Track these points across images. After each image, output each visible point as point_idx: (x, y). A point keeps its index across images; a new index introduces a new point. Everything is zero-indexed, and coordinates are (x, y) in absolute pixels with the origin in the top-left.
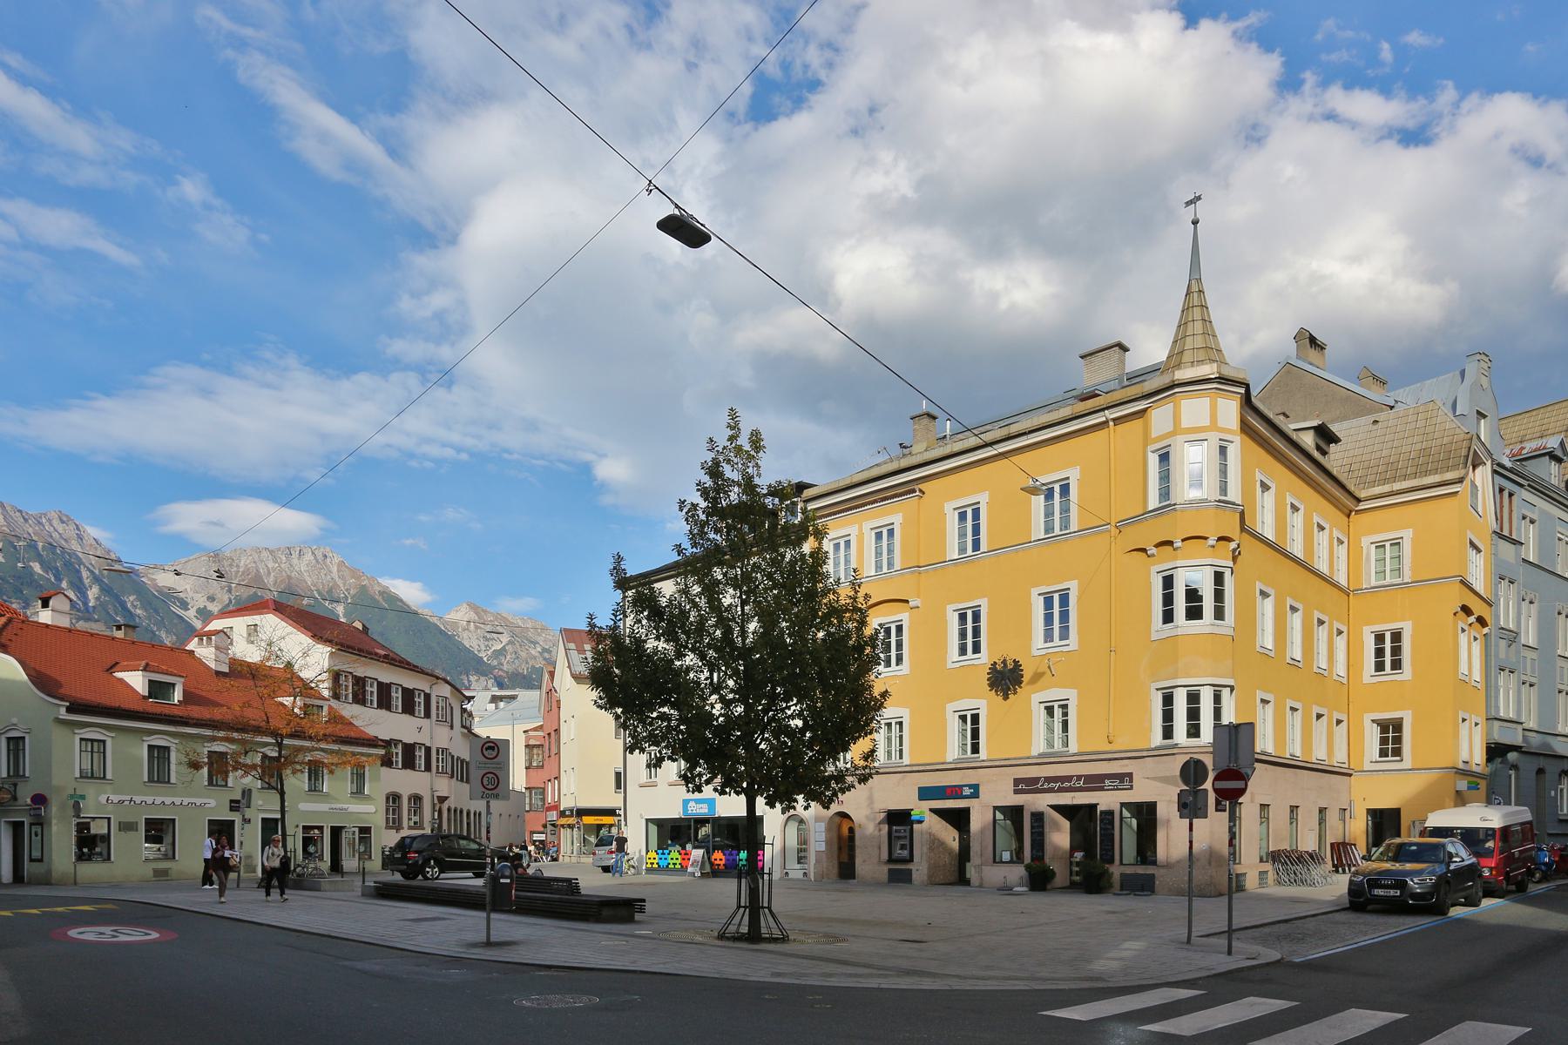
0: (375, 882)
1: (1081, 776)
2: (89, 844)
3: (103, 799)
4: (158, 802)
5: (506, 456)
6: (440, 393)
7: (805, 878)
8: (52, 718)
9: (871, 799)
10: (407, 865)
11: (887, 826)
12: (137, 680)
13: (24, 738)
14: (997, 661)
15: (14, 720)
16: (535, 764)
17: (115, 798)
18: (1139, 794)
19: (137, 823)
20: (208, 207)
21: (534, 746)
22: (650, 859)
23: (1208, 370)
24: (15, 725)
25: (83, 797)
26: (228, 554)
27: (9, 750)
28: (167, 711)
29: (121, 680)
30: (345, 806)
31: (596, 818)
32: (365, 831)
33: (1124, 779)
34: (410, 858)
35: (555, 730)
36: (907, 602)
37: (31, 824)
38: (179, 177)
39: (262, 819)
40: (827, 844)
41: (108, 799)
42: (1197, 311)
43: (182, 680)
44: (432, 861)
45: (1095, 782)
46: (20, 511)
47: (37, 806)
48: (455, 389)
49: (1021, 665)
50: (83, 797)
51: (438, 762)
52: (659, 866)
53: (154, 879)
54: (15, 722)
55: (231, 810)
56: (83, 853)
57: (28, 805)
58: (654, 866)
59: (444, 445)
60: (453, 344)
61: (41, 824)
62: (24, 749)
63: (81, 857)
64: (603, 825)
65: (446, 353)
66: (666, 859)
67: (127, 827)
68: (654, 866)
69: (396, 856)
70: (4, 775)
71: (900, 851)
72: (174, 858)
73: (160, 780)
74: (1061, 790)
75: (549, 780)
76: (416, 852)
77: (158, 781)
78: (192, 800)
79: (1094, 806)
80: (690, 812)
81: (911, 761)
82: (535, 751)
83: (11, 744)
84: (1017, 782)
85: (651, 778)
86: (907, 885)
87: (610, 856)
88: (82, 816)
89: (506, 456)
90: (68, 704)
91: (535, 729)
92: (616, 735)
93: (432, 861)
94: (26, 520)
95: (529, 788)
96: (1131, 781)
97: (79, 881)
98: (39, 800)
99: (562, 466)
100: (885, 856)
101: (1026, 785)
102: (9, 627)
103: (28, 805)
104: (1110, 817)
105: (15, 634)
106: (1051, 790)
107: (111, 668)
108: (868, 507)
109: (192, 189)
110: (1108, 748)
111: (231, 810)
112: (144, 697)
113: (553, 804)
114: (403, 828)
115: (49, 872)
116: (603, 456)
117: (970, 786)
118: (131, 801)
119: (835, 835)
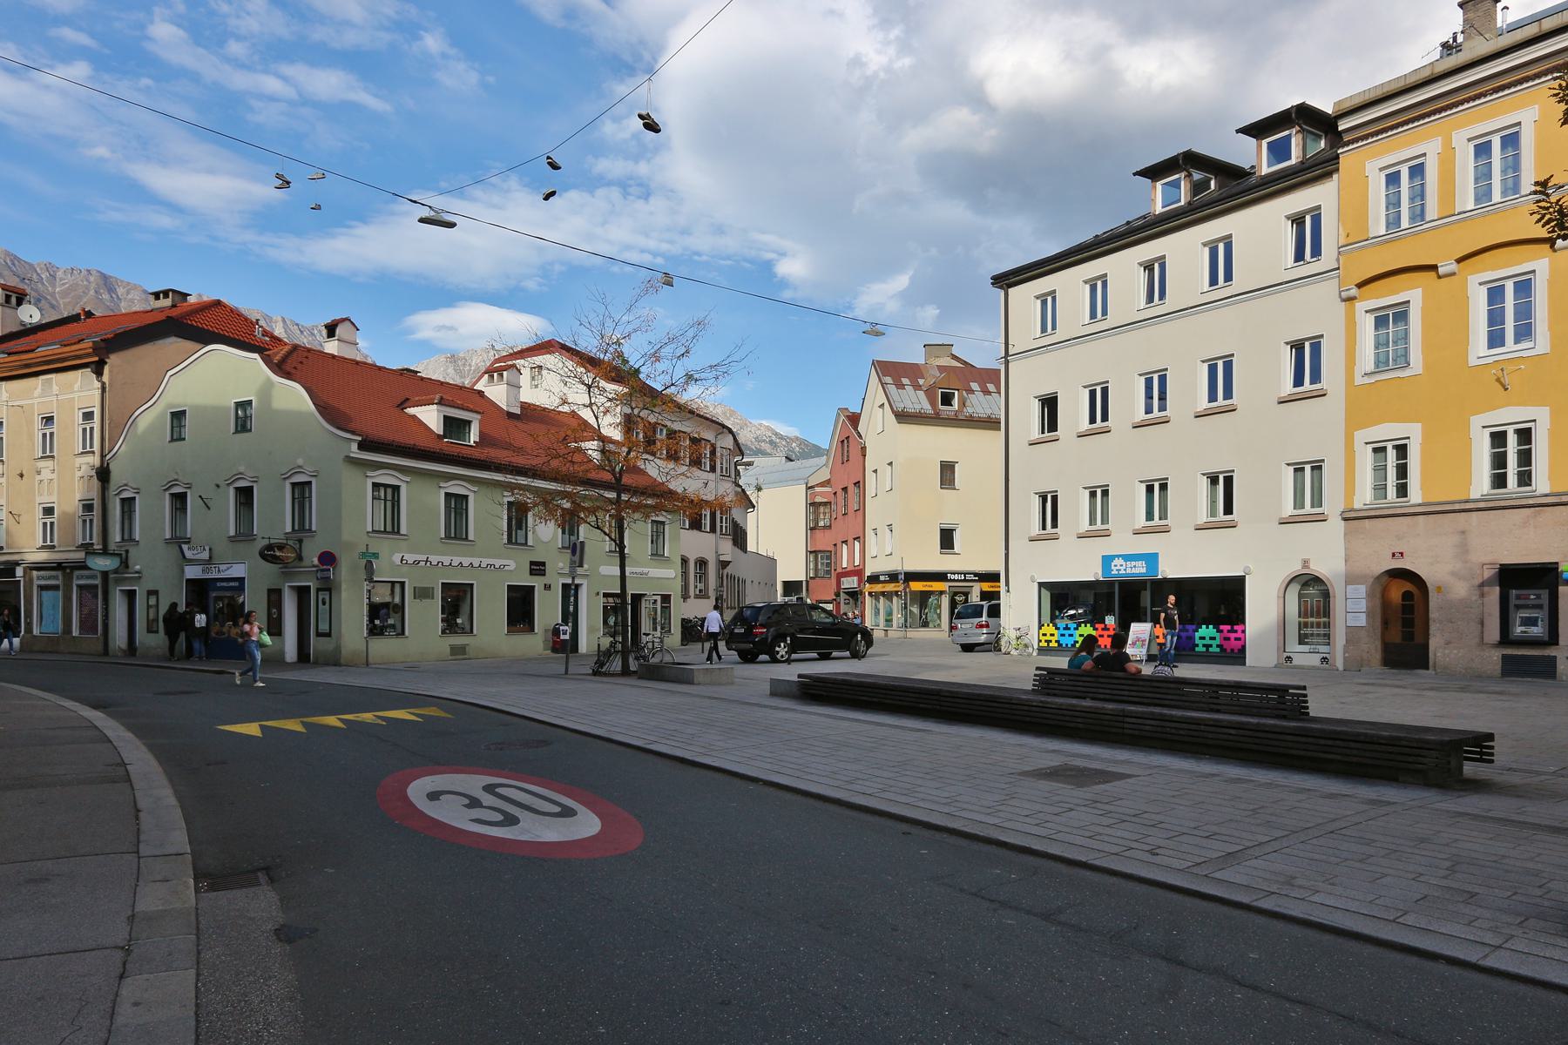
0: (800, 676)
2: (383, 618)
3: (397, 558)
4: (454, 563)
5: (696, 258)
6: (640, 204)
7: (1325, 665)
8: (342, 456)
9: (1463, 549)
10: (754, 643)
11: (1497, 589)
12: (431, 416)
13: (310, 483)
15: (300, 462)
16: (821, 524)
17: (410, 558)
19: (433, 588)
20: (444, 56)
21: (821, 504)
22: (1044, 635)
24: (300, 467)
25: (376, 556)
26: (461, 355)
27: (293, 499)
28: (465, 452)
29: (414, 417)
30: (646, 570)
31: (925, 583)
32: (666, 599)
34: (756, 635)
35: (857, 484)
36: (1434, 268)
37: (318, 590)
38: (422, 32)
39: (563, 584)
40: (1368, 616)
41: (402, 560)
43: (479, 417)
44: (859, 636)
46: (297, 325)
47: (325, 567)
48: (652, 200)
50: (376, 556)
51: (721, 522)
52: (1060, 645)
53: (450, 658)
54: (300, 464)
55: (531, 574)
56: (376, 625)
57: (314, 566)
58: (1051, 645)
59: (642, 251)
60: (649, 161)
61: (329, 590)
62: (310, 497)
63: (374, 631)
64: (931, 593)
65: (643, 169)
66: (1071, 635)
67: (423, 593)
68: (1051, 645)
69: (736, 631)
70: (289, 529)
71: (1523, 629)
72: (472, 631)
73: (458, 536)
75: (845, 542)
76: (762, 626)
77: (455, 538)
78: (491, 561)
80: (1114, 572)
81: (1423, 498)
82: (822, 509)
83: (296, 491)
86: (1550, 681)
87: (979, 631)
88: (375, 579)
89: (696, 258)
90: (360, 439)
91: (822, 485)
92: (941, 484)
93: (859, 636)
94: (302, 332)
95: (814, 552)
97: (370, 660)
98: (328, 559)
99: (747, 265)
100: (1493, 633)
102: (295, 354)
103: (314, 566)
105: (301, 363)
107: (402, 404)
108: (1466, 106)
109: (433, 42)
111: (531, 574)
112: (439, 436)
113: (851, 568)
114: (690, 597)
115: (338, 649)
116: (783, 254)
118: (427, 561)
119: (1378, 602)
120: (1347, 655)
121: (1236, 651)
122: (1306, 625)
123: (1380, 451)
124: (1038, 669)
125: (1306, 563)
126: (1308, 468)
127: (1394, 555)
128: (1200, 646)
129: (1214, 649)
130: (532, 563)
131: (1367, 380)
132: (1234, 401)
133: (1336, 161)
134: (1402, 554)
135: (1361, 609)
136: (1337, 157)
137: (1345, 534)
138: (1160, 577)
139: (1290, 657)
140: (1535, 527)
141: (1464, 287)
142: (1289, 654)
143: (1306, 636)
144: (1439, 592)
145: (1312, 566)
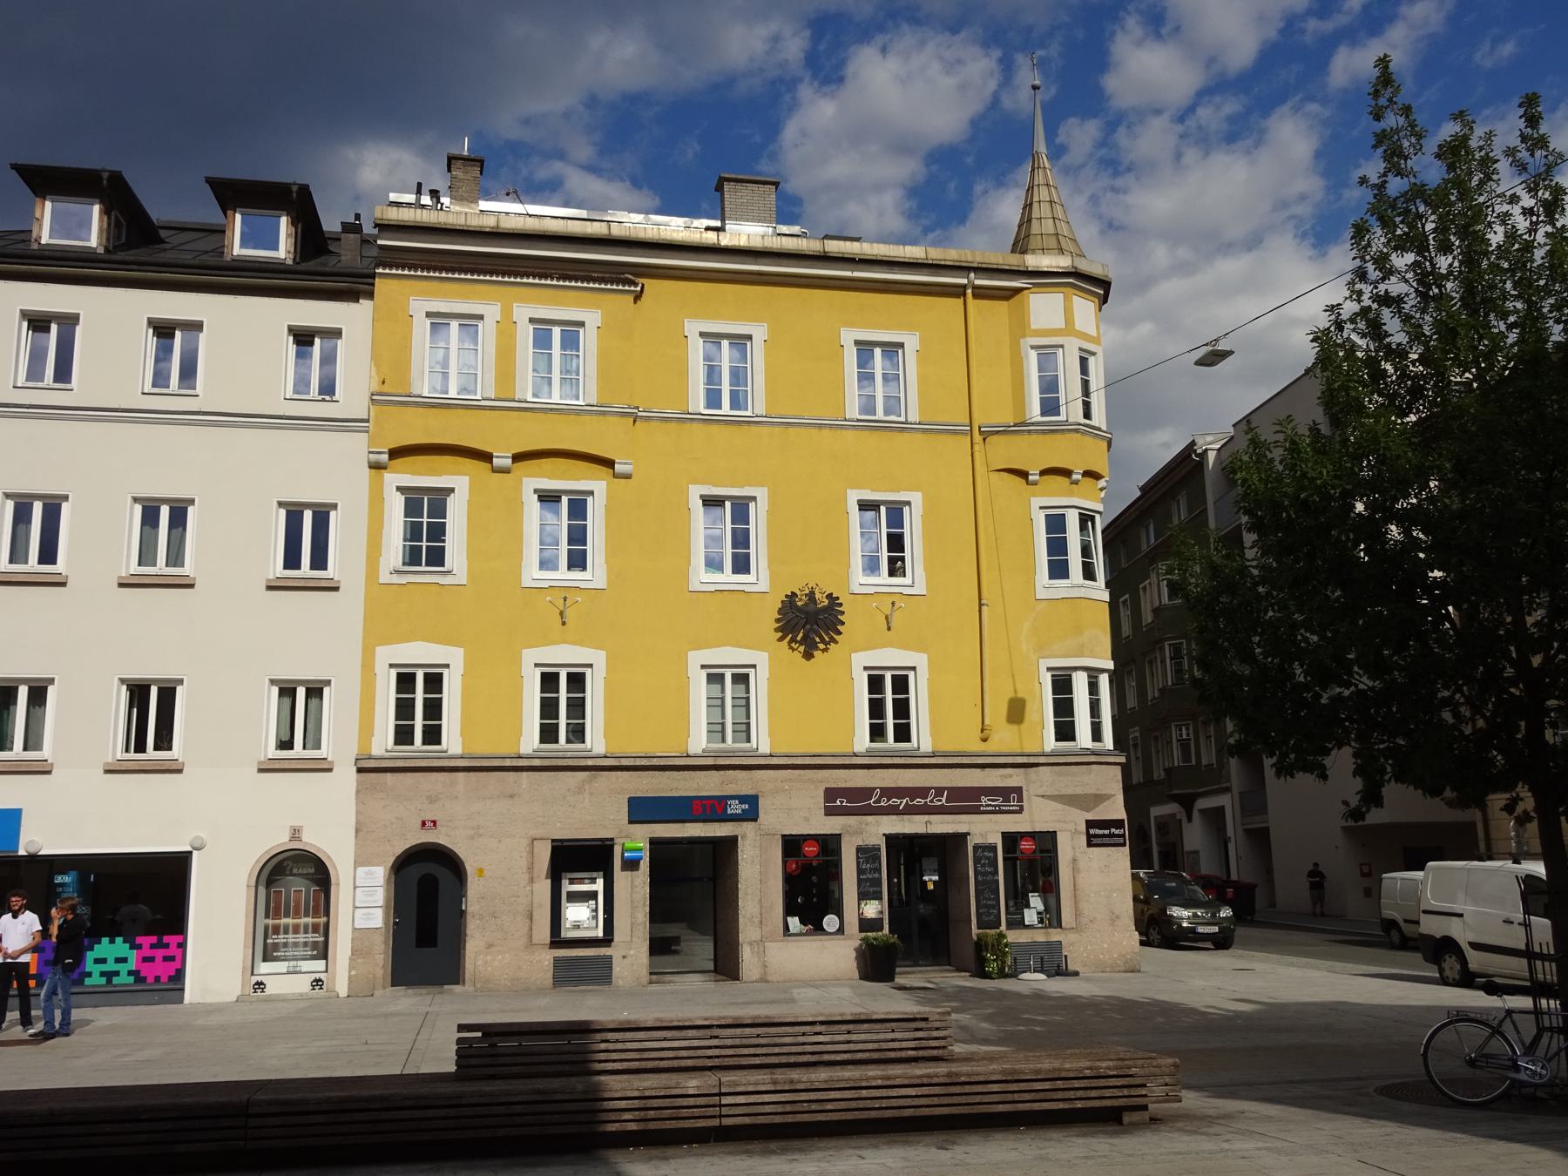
1: (943, 789)
14: (798, 592)
18: (1036, 816)
23: (1062, 262)
33: (1010, 797)
36: (609, 464)
42: (1044, 191)
45: (965, 800)
49: (841, 605)
74: (910, 811)
79: (961, 838)
81: (463, 748)
84: (831, 794)
85: (140, 747)
96: (1020, 799)
100: (543, 932)
101: (842, 801)
104: (991, 855)
106: (893, 811)
110: (976, 746)
117: (742, 799)
120: (353, 973)
121: (164, 979)
122: (276, 930)
123: (715, 679)
124: (462, 1028)
125: (296, 833)
126: (301, 693)
127: (424, 824)
128: (96, 974)
129: (124, 979)
130: (1090, 824)
131: (396, 579)
132: (61, 566)
133: (370, 280)
134: (434, 822)
135: (375, 901)
136: (373, 276)
137: (358, 792)
138: (22, 852)
139: (262, 983)
140: (591, 794)
141: (518, 488)
142: (259, 979)
143: (276, 947)
144: (480, 876)
145: (304, 839)
